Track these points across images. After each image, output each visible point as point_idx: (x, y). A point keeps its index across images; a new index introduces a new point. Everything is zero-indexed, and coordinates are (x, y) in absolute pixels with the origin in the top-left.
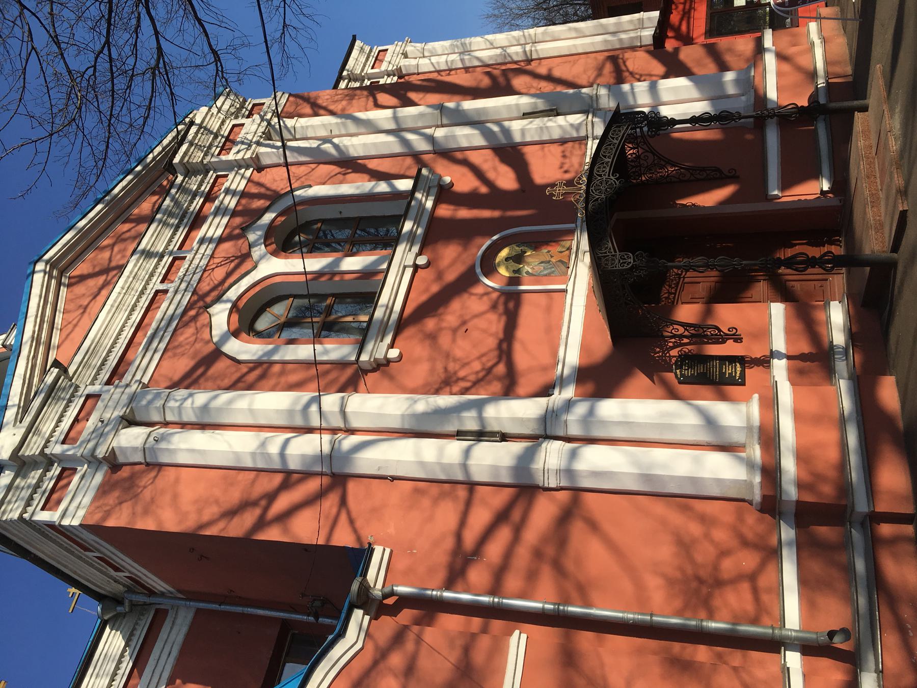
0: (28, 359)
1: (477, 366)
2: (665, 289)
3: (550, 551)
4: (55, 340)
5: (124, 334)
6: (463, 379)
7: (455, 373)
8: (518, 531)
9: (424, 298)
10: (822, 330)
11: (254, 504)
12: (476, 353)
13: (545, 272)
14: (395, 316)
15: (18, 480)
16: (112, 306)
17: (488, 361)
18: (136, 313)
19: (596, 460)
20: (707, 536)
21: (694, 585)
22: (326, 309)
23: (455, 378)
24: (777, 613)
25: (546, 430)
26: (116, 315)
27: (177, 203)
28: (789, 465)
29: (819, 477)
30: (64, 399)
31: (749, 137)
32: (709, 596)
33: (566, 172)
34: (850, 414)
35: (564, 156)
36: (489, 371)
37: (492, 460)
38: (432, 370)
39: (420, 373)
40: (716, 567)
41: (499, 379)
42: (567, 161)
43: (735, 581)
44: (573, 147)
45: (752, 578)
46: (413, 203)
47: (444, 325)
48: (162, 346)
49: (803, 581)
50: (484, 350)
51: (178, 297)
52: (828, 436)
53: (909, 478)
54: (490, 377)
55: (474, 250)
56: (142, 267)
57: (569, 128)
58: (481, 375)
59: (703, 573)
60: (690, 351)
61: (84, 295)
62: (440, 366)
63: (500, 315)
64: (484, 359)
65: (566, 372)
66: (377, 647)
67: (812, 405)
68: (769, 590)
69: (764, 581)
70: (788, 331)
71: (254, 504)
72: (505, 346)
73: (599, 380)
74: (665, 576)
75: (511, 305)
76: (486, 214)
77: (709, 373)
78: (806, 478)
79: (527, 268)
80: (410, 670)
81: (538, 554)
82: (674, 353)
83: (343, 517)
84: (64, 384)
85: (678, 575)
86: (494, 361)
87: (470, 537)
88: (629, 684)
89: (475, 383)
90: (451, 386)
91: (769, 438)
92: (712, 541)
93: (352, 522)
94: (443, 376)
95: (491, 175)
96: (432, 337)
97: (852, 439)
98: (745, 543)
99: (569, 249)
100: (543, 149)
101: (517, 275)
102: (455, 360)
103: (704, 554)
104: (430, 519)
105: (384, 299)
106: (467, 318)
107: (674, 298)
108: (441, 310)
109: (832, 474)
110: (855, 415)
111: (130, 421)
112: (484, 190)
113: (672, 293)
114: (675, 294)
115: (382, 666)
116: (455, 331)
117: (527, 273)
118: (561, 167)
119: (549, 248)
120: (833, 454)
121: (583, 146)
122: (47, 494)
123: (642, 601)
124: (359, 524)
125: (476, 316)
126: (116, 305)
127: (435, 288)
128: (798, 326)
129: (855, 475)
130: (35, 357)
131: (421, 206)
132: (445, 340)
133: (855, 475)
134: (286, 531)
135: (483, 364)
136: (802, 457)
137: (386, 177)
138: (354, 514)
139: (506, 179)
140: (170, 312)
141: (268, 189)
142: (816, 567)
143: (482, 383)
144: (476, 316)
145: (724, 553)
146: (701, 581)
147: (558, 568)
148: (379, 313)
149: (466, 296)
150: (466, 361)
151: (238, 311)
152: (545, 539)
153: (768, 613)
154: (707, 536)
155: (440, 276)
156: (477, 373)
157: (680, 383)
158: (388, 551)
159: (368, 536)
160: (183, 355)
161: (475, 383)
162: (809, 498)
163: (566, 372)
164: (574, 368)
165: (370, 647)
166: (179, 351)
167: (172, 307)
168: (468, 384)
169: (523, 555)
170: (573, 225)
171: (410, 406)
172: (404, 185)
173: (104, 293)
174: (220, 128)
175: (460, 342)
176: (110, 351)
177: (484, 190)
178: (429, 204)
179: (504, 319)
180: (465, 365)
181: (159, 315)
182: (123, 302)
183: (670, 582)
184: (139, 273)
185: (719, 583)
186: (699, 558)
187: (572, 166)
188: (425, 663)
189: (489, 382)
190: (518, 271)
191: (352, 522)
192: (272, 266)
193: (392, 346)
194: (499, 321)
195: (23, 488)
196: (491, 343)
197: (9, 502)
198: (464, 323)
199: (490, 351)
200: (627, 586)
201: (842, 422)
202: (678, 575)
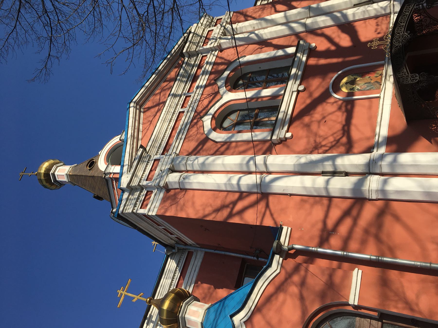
1: (331, 139)
3: (373, 230)
4: (140, 136)
6: (324, 146)
7: (320, 143)
9: (303, 106)
11: (227, 206)
12: (330, 132)
13: (368, 88)
14: (289, 117)
15: (130, 196)
16: (162, 120)
22: (256, 115)
23: (320, 146)
25: (370, 170)
27: (186, 71)
33: (379, 33)
36: (338, 141)
38: (308, 143)
39: (302, 143)
41: (343, 145)
48: (184, 137)
50: (335, 131)
51: (189, 114)
54: (338, 144)
55: (328, 80)
57: (380, 9)
58: (334, 143)
62: (312, 140)
63: (343, 112)
64: (335, 135)
65: (380, 140)
66: (286, 272)
71: (227, 206)
79: (358, 87)
81: (366, 231)
90: (318, 150)
93: (272, 215)
96: (308, 126)
101: (352, 91)
102: (320, 137)
105: (283, 108)
106: (325, 115)
112: (333, 48)
115: (289, 281)
117: (358, 89)
119: (370, 75)
122: (142, 202)
124: (275, 216)
130: (133, 144)
131: (300, 60)
132: (314, 127)
134: (242, 219)
135: (335, 138)
138: (273, 211)
140: (186, 121)
143: (334, 147)
147: (378, 239)
151: (215, 119)
152: (370, 224)
155: (311, 95)
156: (332, 142)
158: (290, 229)
159: (280, 221)
165: (283, 272)
166: (191, 138)
168: (327, 148)
169: (358, 232)
173: (158, 114)
176: (162, 140)
178: (304, 59)
179: (345, 114)
180: (325, 139)
181: (181, 123)
188: (310, 280)
189: (338, 147)
190: (353, 89)
191: (272, 215)
192: (229, 96)
193: (287, 131)
194: (343, 115)
197: (128, 205)
198: (324, 118)
199: (339, 131)
200: (417, 249)
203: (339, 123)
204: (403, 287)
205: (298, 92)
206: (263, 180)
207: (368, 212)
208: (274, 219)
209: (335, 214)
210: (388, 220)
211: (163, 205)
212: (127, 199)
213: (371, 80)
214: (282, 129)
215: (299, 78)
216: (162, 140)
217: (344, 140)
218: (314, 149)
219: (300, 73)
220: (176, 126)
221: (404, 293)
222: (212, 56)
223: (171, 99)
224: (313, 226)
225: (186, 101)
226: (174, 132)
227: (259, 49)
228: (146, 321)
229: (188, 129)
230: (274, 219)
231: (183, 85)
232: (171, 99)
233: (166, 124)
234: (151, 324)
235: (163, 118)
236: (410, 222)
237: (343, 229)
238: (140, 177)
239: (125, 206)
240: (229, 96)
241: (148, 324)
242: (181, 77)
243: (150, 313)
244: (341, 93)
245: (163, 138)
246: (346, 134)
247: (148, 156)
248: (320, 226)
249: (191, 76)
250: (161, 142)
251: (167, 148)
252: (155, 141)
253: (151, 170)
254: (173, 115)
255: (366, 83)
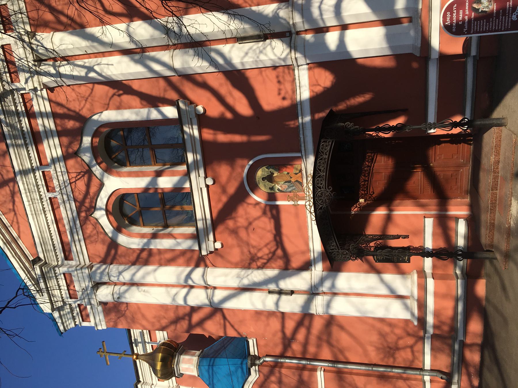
0: (14, 257)
1: (266, 251)
2: (362, 178)
3: (325, 337)
4: (15, 234)
5: (52, 229)
6: (261, 258)
7: (256, 254)
8: (309, 329)
9: (220, 206)
10: (453, 234)
11: (182, 318)
12: (263, 243)
13: (290, 190)
14: (209, 222)
15: (62, 312)
16: (32, 214)
17: (272, 247)
18: (48, 215)
19: (341, 307)
20: (392, 332)
21: (388, 349)
22: (164, 209)
23: (256, 258)
24: (421, 359)
25: (313, 292)
26: (38, 218)
27: (12, 126)
28: (430, 319)
29: (443, 323)
30: (53, 277)
31: (415, 65)
32: (394, 354)
33: (284, 98)
34: (461, 297)
35: (279, 82)
36: (274, 253)
37: (291, 305)
38: (242, 253)
39: (236, 254)
40: (396, 343)
41: (280, 258)
42: (282, 87)
43: (404, 348)
44: (284, 72)
45: (411, 347)
46: (185, 136)
47: (239, 224)
48: (81, 237)
49: (432, 349)
50: (267, 241)
51: (68, 205)
52: (449, 304)
53: (483, 326)
54: (275, 257)
55: (239, 170)
56: (28, 183)
57: (277, 60)
58: (270, 255)
59: (390, 345)
60: (380, 243)
61: (5, 201)
62: (245, 250)
63: (270, 218)
64: (269, 246)
65: (316, 255)
66: (264, 375)
67: (443, 289)
68: (418, 352)
69: (416, 348)
70: (434, 234)
71: (182, 318)
72: (278, 238)
73: (334, 261)
74: (375, 347)
75: (274, 212)
76: (238, 138)
77: (392, 256)
78: (437, 323)
79: (277, 187)
80: (280, 382)
81: (319, 338)
82: (372, 244)
83: (228, 324)
84: (46, 270)
85: (381, 346)
86: (275, 248)
87: (289, 331)
88: (365, 386)
89: (269, 260)
90: (256, 262)
91: (422, 305)
92: (395, 334)
93: (233, 326)
94: (249, 256)
95: (230, 100)
96: (234, 232)
97: (460, 308)
98: (409, 334)
99: (301, 171)
100: (261, 73)
101: (272, 191)
102: (254, 247)
103: (391, 339)
104: (268, 325)
105: (199, 215)
106: (251, 220)
107: (368, 184)
108: (234, 215)
109: (449, 321)
110: (463, 297)
111: (97, 285)
112: (229, 115)
113: (366, 181)
114: (368, 181)
115: (268, 381)
116: (247, 228)
117: (278, 190)
118: (279, 94)
119: (288, 170)
120: (450, 313)
121: (291, 72)
122: (80, 314)
123: (366, 352)
124: (236, 327)
125: (255, 219)
126: (34, 212)
127: (224, 199)
128: (439, 231)
129: (460, 325)
130: (16, 253)
131: (192, 137)
132: (243, 234)
133: (460, 325)
134: (204, 330)
135: (269, 250)
136: (437, 314)
137: (153, 101)
138: (232, 322)
139: (244, 108)
140: (70, 216)
141: (69, 109)
142: (438, 344)
143: (272, 260)
144: (255, 219)
145: (400, 338)
146: (390, 348)
147: (330, 345)
148: (200, 225)
149: (245, 205)
150: (259, 247)
151: (111, 213)
152: (321, 333)
153: (417, 359)
154: (392, 332)
155: (224, 190)
156: (268, 254)
157: (376, 262)
158: (255, 340)
159: (244, 334)
160: (96, 242)
161: (269, 260)
162: (437, 332)
163: (316, 255)
164: (318, 253)
165: (261, 375)
166: (93, 239)
167: (69, 213)
168: (265, 261)
169: (313, 339)
170: (299, 155)
171: (240, 281)
172: (171, 112)
173: (17, 199)
174: (31, 164)
175: (252, 236)
176: (52, 239)
177: (229, 115)
178: (196, 133)
179: (272, 221)
180: (260, 250)
181: (65, 221)
182: (36, 210)
183: (378, 349)
184: (30, 188)
185: (398, 349)
186: (389, 340)
187: (287, 92)
188: (285, 380)
189: (276, 260)
190: (272, 188)
191: (233, 326)
192: (114, 183)
193: (215, 241)
194: (270, 222)
195: (66, 314)
196: (270, 237)
197: (66, 322)
198: (250, 224)
199: (271, 242)
200: (360, 350)
201: (457, 300)
202: (381, 346)
203: (269, 231)
204: (354, 380)
205: (207, 186)
206: (211, 301)
207: (317, 325)
208: (236, 330)
209: (290, 325)
210: (335, 330)
211: (109, 318)
212: (61, 317)
213: (291, 178)
214: (208, 240)
215: (201, 164)
216: (52, 239)
217: (279, 252)
218: (251, 261)
219: (199, 157)
220: (57, 217)
221: (355, 384)
222: (41, 100)
223: (23, 181)
224: (274, 335)
225: (47, 178)
226: (60, 226)
227: (115, 97)
228: (134, 345)
229: (81, 226)
230: (236, 330)
231: (24, 152)
232: (23, 181)
233: (42, 217)
234: (140, 344)
235: (31, 211)
236: (351, 330)
237: (301, 336)
238: (60, 295)
239: (63, 323)
240: (114, 183)
241: (136, 346)
242: (11, 139)
243: (133, 339)
244: (260, 191)
245: (51, 237)
246: (280, 245)
247: (50, 269)
248: (280, 335)
249: (27, 136)
250: (53, 242)
251: (66, 248)
252: (43, 243)
253: (68, 286)
254: (42, 202)
255: (286, 182)
